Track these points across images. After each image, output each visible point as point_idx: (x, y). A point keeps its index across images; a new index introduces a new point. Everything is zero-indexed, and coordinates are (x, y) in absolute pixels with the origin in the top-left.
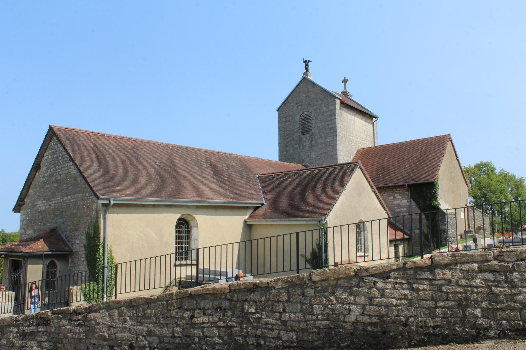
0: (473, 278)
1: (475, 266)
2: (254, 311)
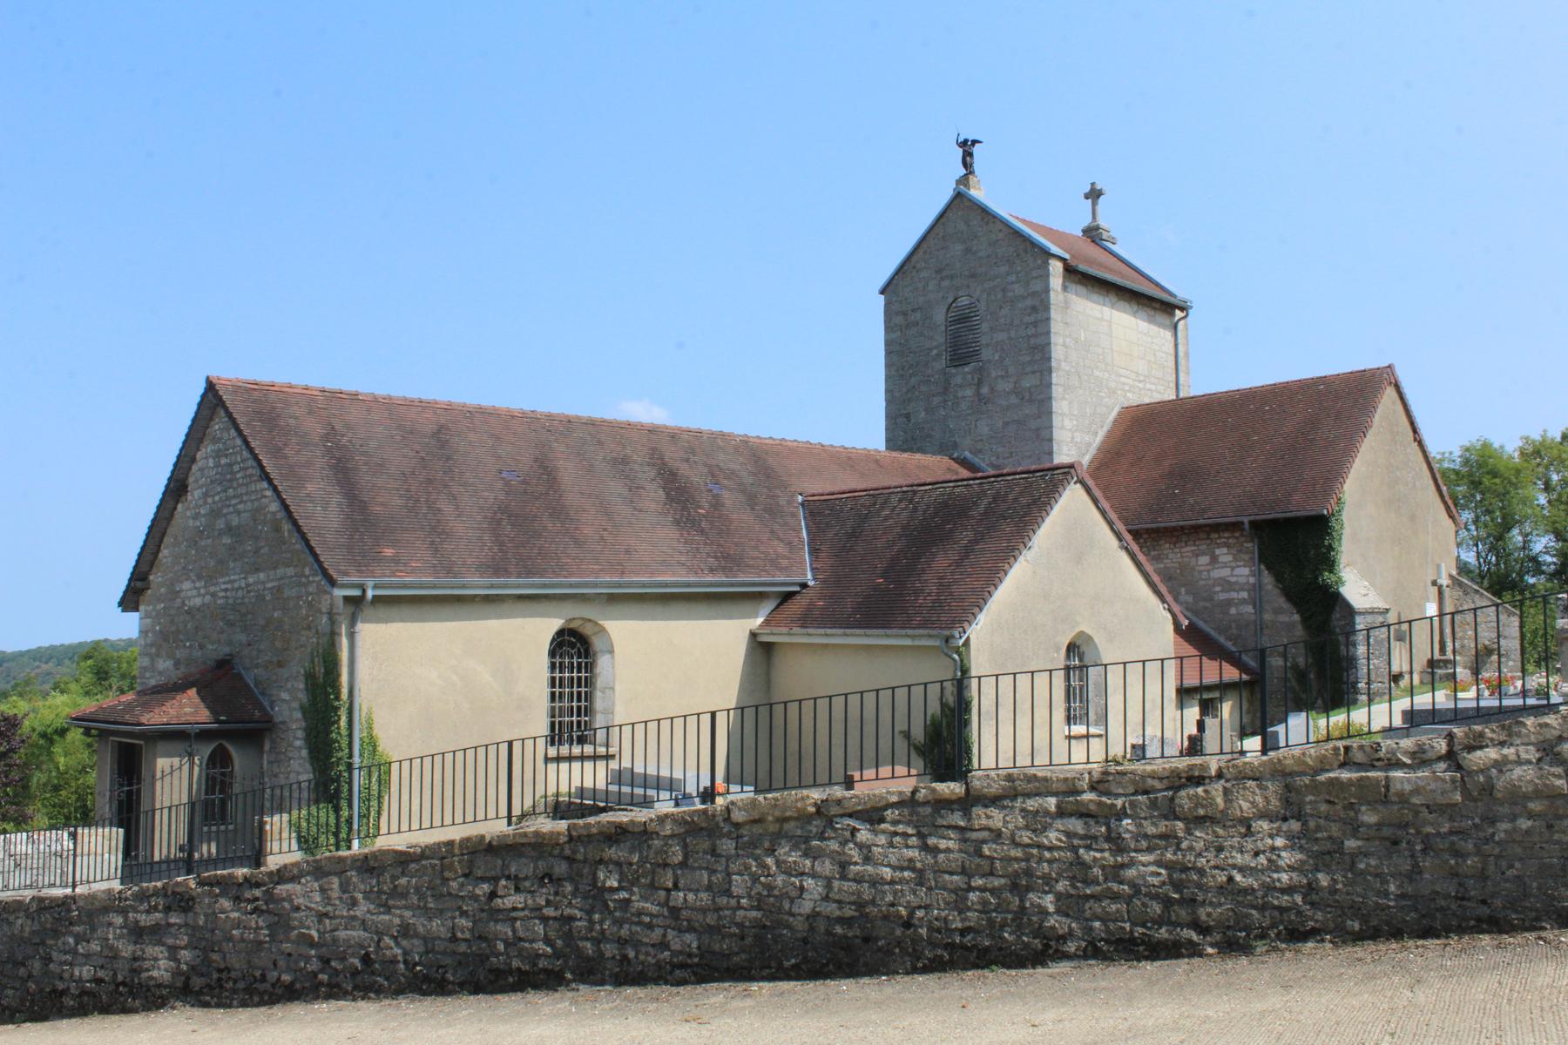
0: (1045, 829)
1: (1051, 803)
2: (616, 884)
